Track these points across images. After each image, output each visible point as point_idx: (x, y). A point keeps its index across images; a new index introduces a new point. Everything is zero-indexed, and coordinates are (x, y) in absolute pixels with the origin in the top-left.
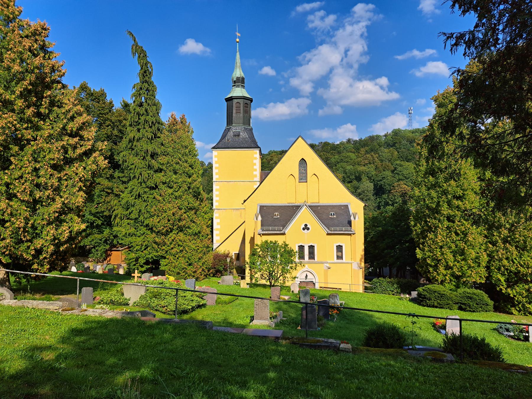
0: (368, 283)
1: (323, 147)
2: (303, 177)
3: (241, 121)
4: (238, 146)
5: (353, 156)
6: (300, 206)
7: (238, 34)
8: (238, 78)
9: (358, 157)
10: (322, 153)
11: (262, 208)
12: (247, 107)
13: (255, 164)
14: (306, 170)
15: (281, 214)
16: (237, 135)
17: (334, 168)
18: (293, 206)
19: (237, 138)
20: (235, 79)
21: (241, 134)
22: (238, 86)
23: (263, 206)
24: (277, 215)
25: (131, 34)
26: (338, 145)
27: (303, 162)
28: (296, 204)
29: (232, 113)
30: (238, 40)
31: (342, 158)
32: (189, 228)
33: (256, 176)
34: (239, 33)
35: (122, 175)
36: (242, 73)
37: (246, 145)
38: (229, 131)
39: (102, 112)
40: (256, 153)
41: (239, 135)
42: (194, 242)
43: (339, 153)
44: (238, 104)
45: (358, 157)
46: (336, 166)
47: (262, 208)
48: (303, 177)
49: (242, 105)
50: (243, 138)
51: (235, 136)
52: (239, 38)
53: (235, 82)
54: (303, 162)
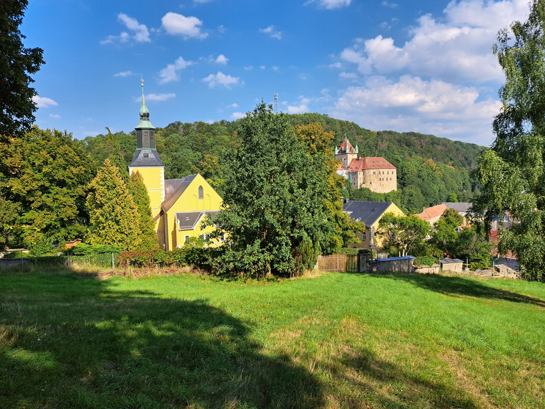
0: (156, 295)
1: (198, 127)
2: (201, 196)
3: (149, 145)
4: (148, 165)
5: (226, 138)
6: (199, 213)
7: (142, 80)
8: (144, 114)
9: (231, 140)
10: (198, 134)
11: (178, 214)
12: (152, 135)
13: (161, 177)
14: (202, 192)
15: (190, 218)
16: (146, 156)
17: (210, 150)
18: (196, 213)
19: (146, 158)
20: (142, 114)
21: (149, 155)
22: (145, 120)
23: (179, 214)
24: (188, 219)
25: (107, 128)
26: (212, 125)
27: (201, 188)
28: (198, 212)
29: (142, 139)
30: (142, 85)
31: (217, 140)
32: (147, 231)
33: (162, 185)
34: (143, 79)
35: (70, 191)
36: (147, 110)
37: (154, 164)
38: (140, 152)
39: (54, 148)
40: (162, 169)
41: (148, 156)
42: (149, 238)
43: (214, 134)
44: (146, 134)
45: (231, 140)
46: (212, 148)
47: (178, 214)
48: (201, 196)
49: (149, 134)
50: (151, 158)
51: (145, 156)
52: (143, 83)
53: (142, 116)
54: (201, 188)
